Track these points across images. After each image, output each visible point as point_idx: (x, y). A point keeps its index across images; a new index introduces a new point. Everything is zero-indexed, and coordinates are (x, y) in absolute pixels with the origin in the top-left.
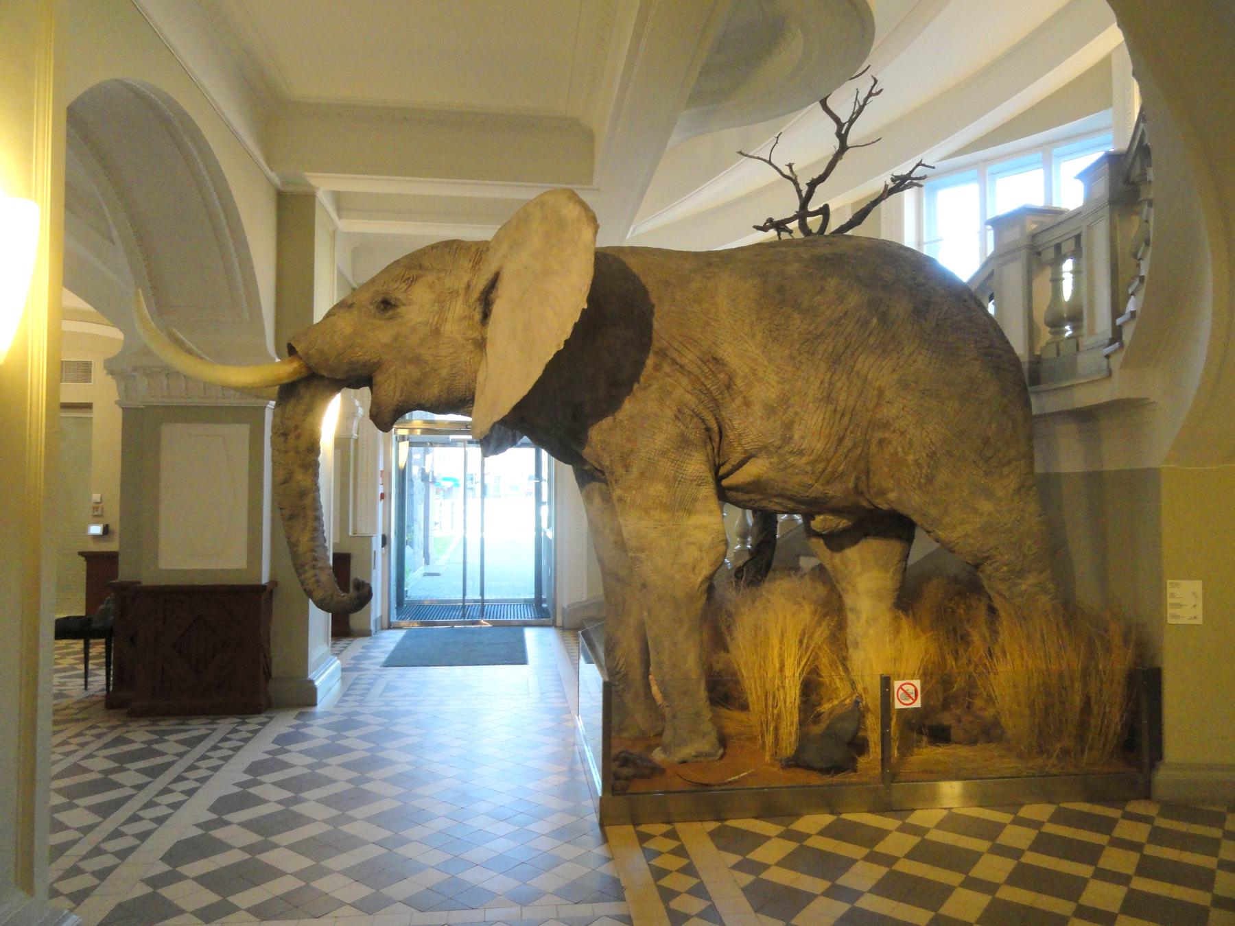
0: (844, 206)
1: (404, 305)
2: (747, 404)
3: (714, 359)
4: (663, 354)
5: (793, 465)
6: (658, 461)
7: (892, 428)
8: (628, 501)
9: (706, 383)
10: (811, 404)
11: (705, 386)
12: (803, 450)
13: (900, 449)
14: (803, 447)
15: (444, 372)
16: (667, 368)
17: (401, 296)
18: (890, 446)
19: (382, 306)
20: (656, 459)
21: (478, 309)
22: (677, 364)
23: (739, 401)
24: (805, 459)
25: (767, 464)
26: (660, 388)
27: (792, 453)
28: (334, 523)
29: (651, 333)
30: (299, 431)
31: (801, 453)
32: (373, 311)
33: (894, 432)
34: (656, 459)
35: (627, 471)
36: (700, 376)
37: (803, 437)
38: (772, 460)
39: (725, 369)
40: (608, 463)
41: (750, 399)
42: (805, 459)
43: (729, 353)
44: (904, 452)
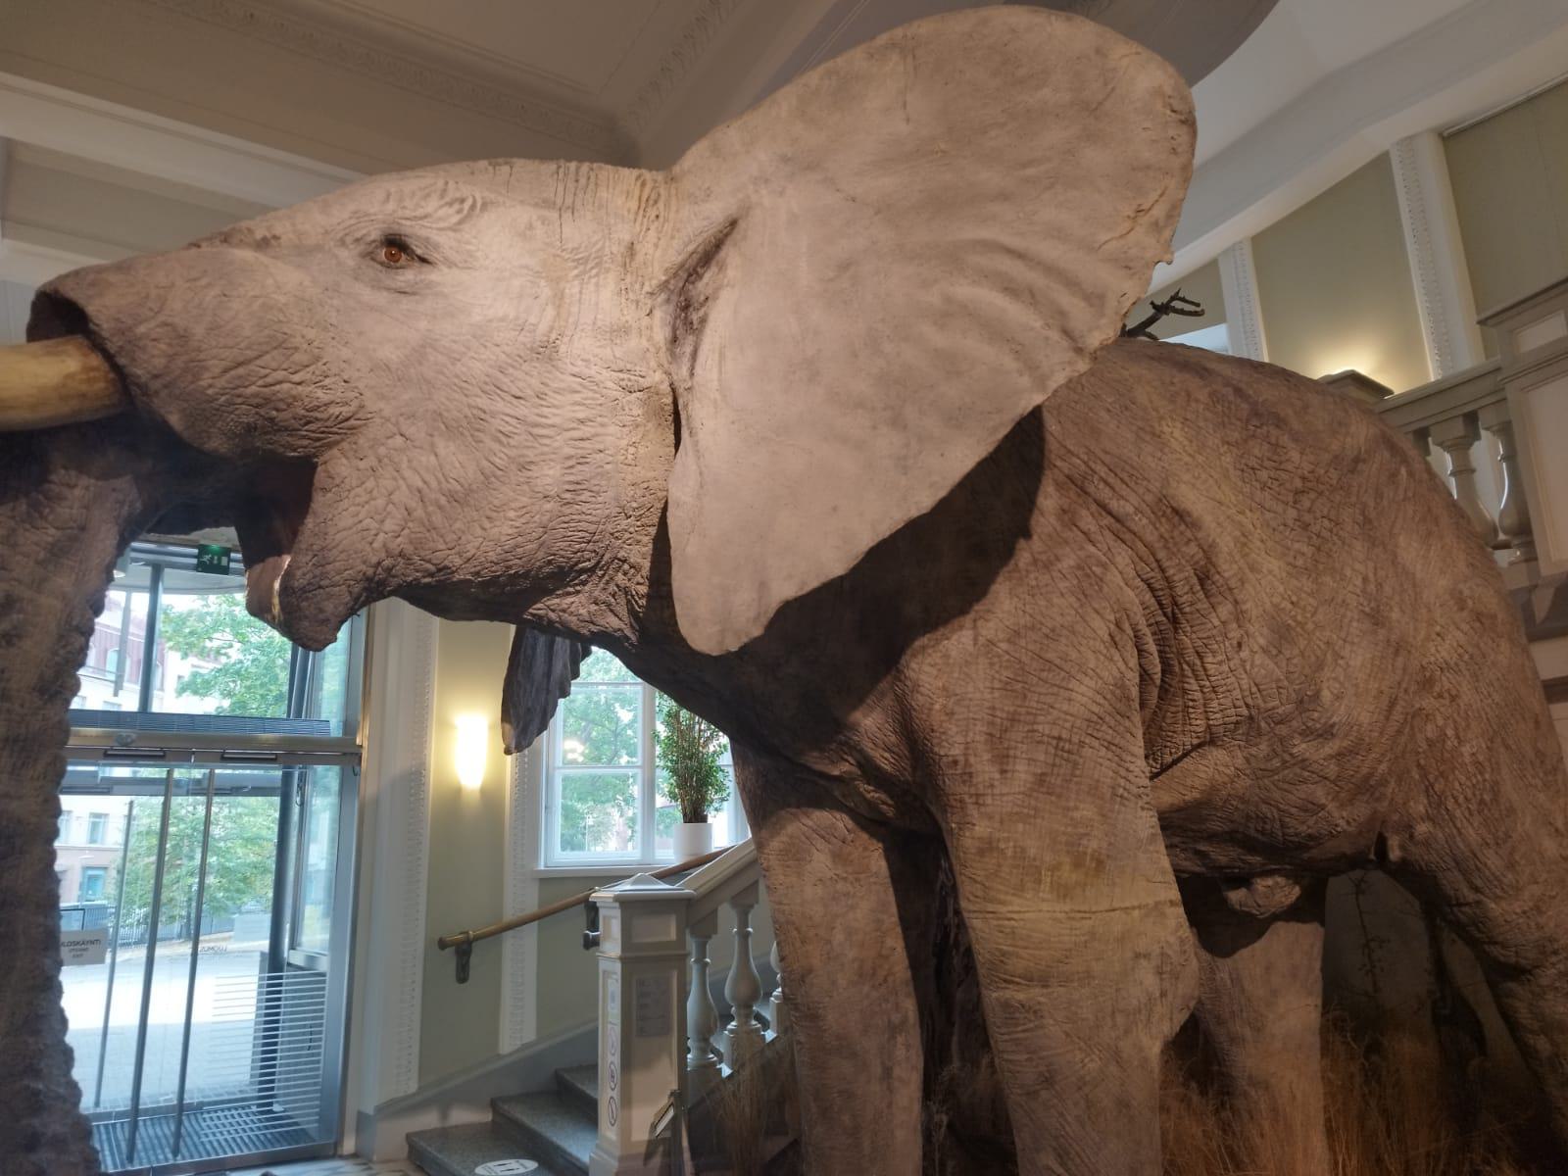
0: (1241, 242)
1: (451, 264)
2: (1239, 617)
3: (1175, 511)
4: (1077, 485)
5: (1303, 763)
6: (1082, 744)
7: (1437, 689)
8: (1010, 853)
9: (1166, 564)
10: (1355, 624)
11: (1163, 571)
12: (1333, 726)
13: (1450, 732)
14: (1335, 719)
15: (549, 476)
16: (1087, 520)
17: (444, 240)
18: (1429, 727)
19: (382, 254)
20: (1075, 739)
21: (658, 314)
22: (1110, 513)
23: (1225, 610)
24: (1331, 747)
25: (1240, 761)
26: (1079, 567)
27: (1307, 733)
28: (253, 940)
29: (1042, 439)
30: (16, 617)
31: (1327, 733)
32: (351, 263)
33: (1440, 696)
34: (1075, 739)
35: (1003, 772)
36: (1157, 545)
37: (1338, 697)
38: (1253, 751)
39: (1200, 535)
40: (956, 751)
41: (1244, 607)
42: (1331, 747)
43: (1191, 498)
44: (1458, 737)
